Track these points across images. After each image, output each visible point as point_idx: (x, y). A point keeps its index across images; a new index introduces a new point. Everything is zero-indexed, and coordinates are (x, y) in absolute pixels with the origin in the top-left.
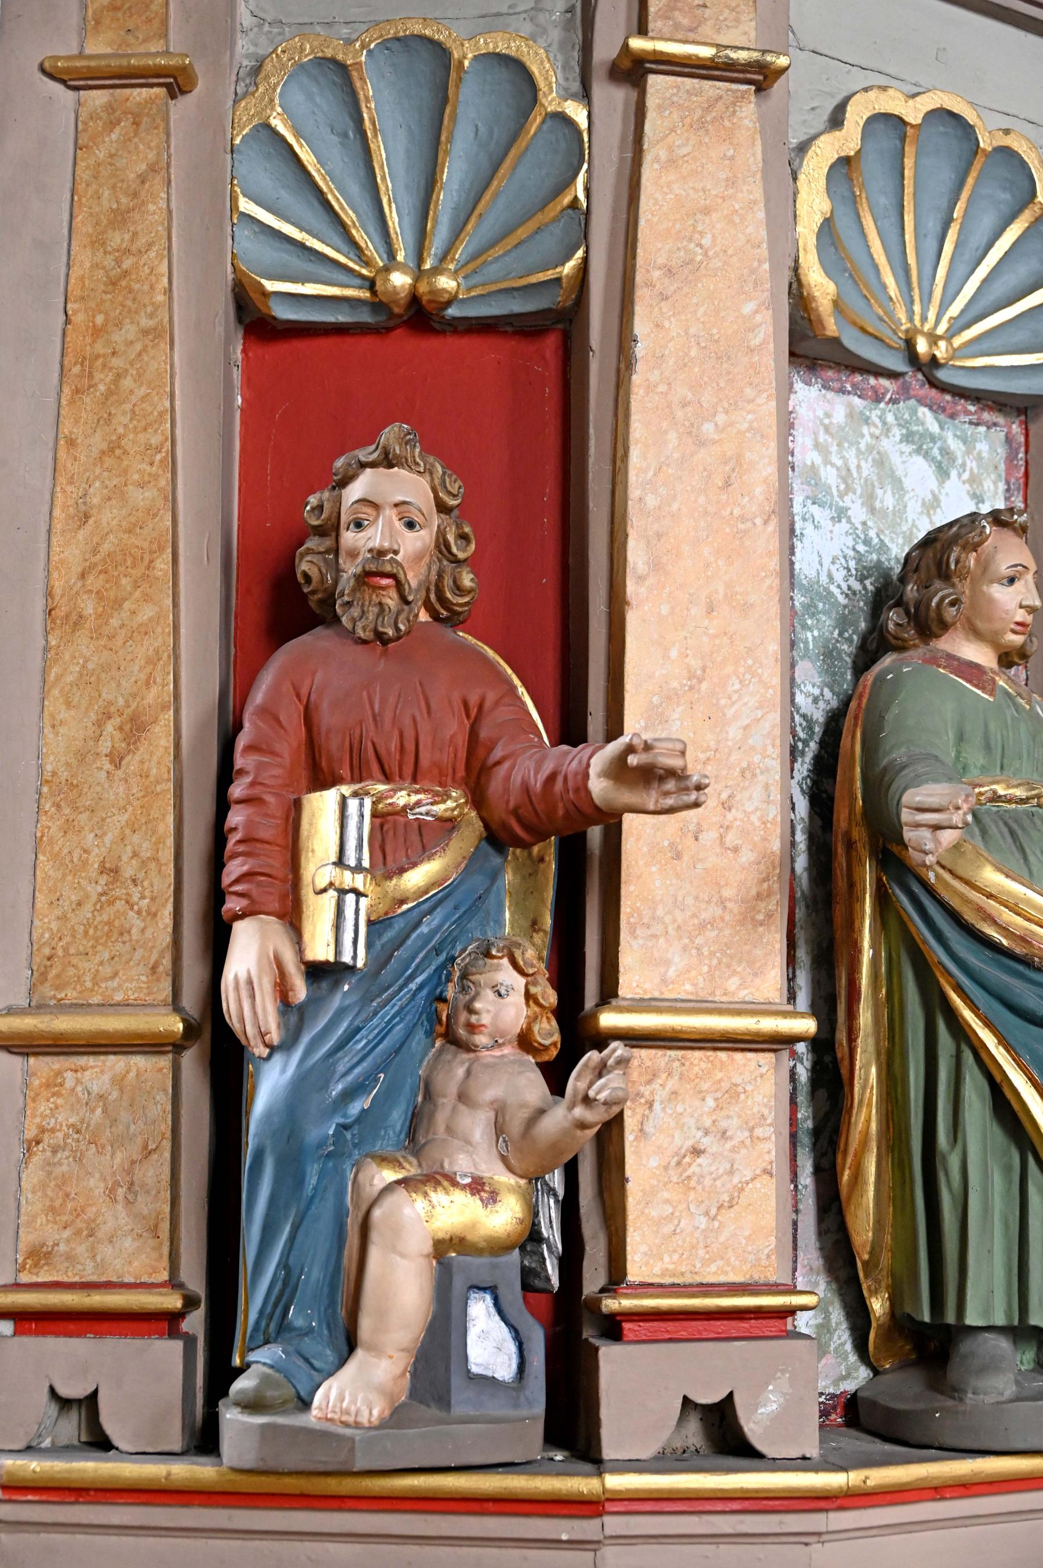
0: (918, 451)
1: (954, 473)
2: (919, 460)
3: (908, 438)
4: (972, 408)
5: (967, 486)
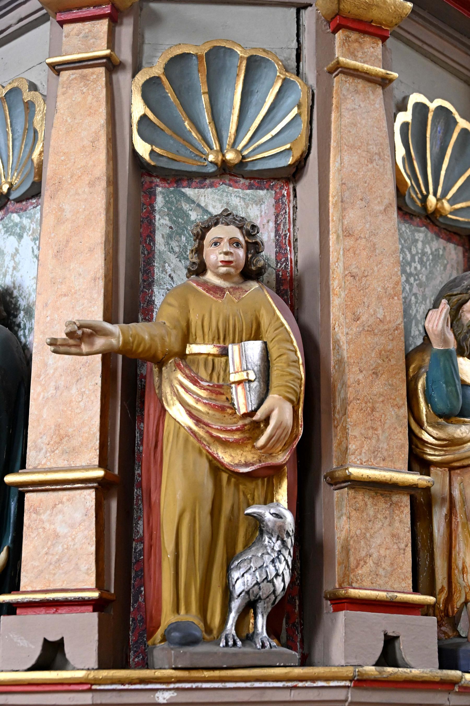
0: (10, 235)
1: (25, 235)
2: (12, 238)
3: (6, 232)
4: (34, 201)
5: (31, 237)
